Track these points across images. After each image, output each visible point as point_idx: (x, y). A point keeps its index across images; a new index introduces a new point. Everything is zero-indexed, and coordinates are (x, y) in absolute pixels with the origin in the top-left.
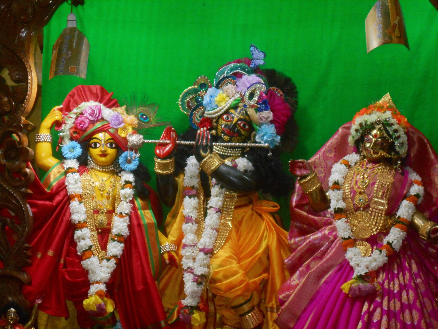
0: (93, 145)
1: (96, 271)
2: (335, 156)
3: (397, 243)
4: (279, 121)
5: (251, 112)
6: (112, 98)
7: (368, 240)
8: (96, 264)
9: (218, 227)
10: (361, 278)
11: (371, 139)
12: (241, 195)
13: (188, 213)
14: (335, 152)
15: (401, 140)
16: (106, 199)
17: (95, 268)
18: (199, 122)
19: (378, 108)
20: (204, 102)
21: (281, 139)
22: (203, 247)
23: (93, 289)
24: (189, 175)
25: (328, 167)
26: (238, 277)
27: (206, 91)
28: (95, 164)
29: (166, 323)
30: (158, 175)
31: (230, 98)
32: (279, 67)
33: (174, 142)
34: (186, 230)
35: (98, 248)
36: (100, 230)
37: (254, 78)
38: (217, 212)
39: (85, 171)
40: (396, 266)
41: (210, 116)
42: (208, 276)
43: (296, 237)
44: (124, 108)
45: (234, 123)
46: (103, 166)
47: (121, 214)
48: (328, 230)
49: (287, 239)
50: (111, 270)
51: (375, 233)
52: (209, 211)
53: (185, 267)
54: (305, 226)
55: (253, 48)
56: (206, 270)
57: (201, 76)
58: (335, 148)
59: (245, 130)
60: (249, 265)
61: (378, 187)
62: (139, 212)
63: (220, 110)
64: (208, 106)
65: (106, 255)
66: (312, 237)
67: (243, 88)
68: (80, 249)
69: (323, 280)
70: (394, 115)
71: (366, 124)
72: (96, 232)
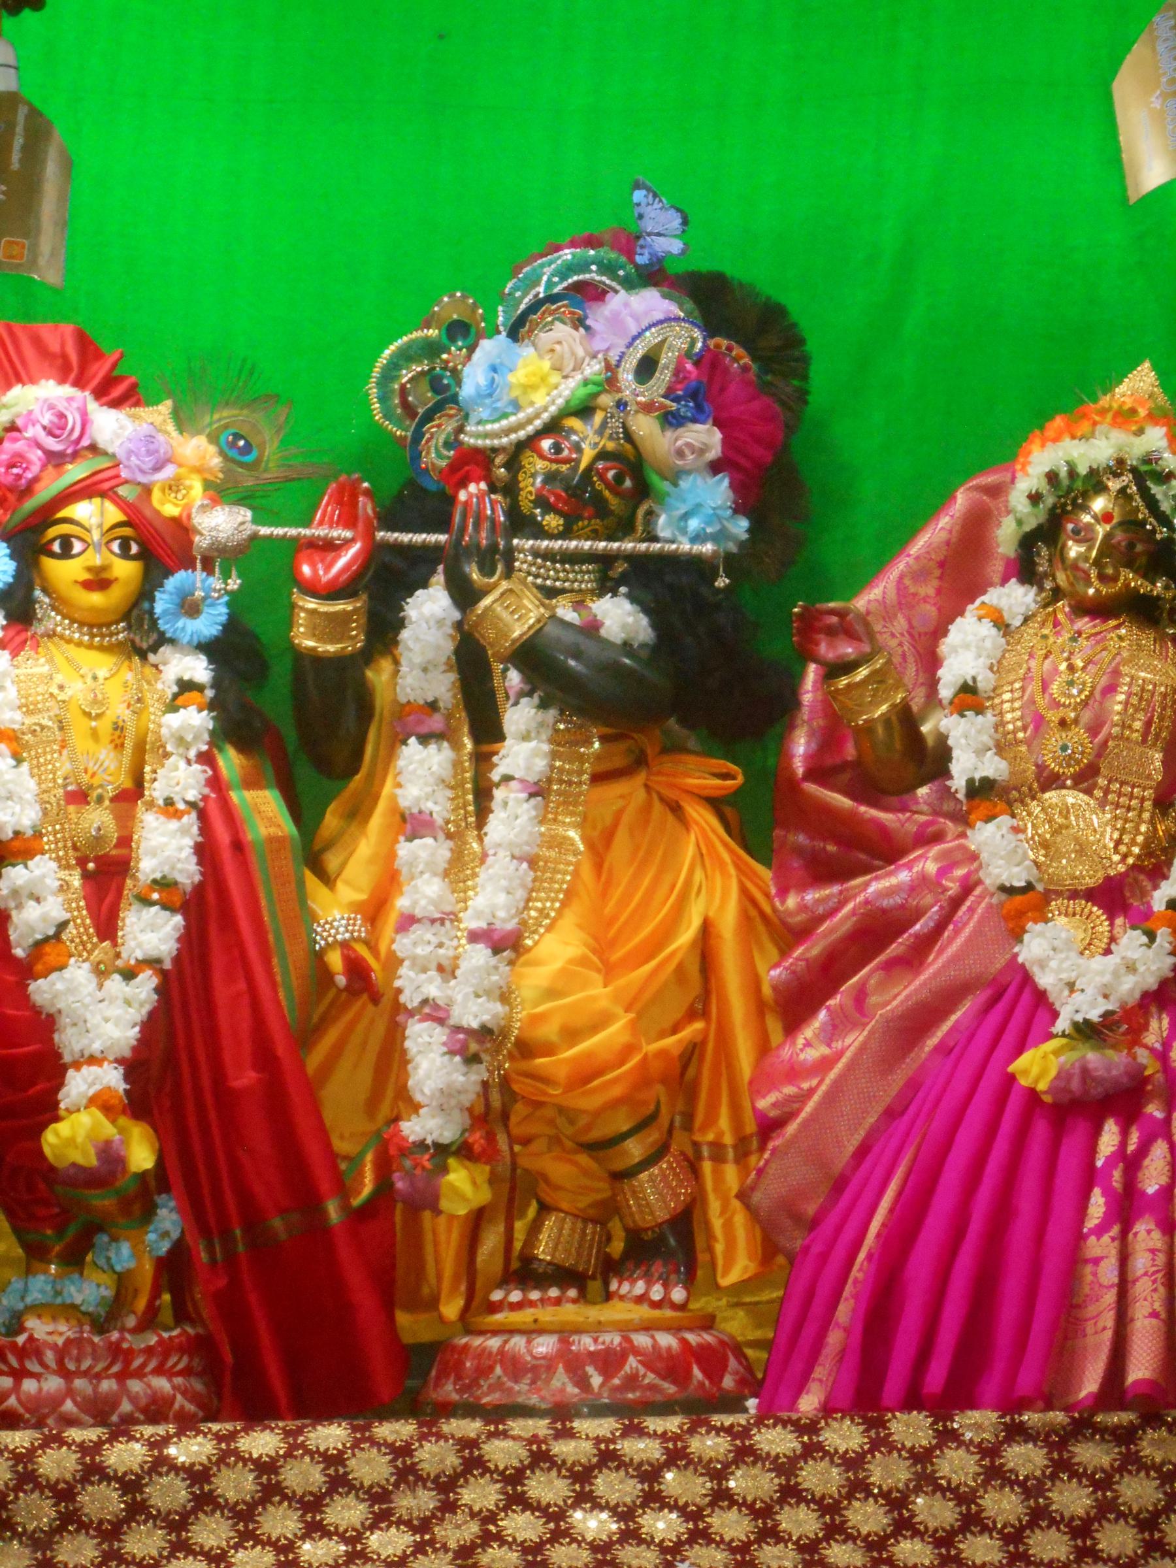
0: (56, 547)
1: (88, 1016)
2: (939, 591)
4: (744, 462)
5: (645, 427)
9: (536, 850)
10: (1086, 1031)
11: (1089, 527)
13: (418, 799)
14: (940, 578)
17: (86, 1006)
18: (443, 463)
20: (467, 391)
21: (749, 531)
23: (78, 1085)
24: (418, 660)
26: (614, 1033)
27: (472, 349)
28: (64, 617)
29: (345, 1206)
30: (302, 658)
31: (565, 377)
32: (755, 271)
33: (369, 535)
34: (411, 865)
35: (86, 930)
36: (91, 866)
37: (651, 303)
38: (532, 795)
39: (25, 642)
42: (505, 1032)
43: (803, 888)
44: (166, 407)
45: (583, 466)
46: (91, 626)
47: (169, 802)
48: (936, 859)
49: (767, 895)
50: (138, 1014)
51: (1121, 868)
52: (499, 794)
53: (410, 999)
54: (831, 848)
55: (644, 192)
56: (499, 1008)
57: (452, 296)
58: (941, 565)
59: (618, 491)
60: (642, 990)
61: (1126, 703)
62: (235, 796)
63: (529, 421)
64: (483, 405)
65: (118, 955)
66: (883, 886)
68: (21, 936)
69: (932, 1042)
72: (77, 873)
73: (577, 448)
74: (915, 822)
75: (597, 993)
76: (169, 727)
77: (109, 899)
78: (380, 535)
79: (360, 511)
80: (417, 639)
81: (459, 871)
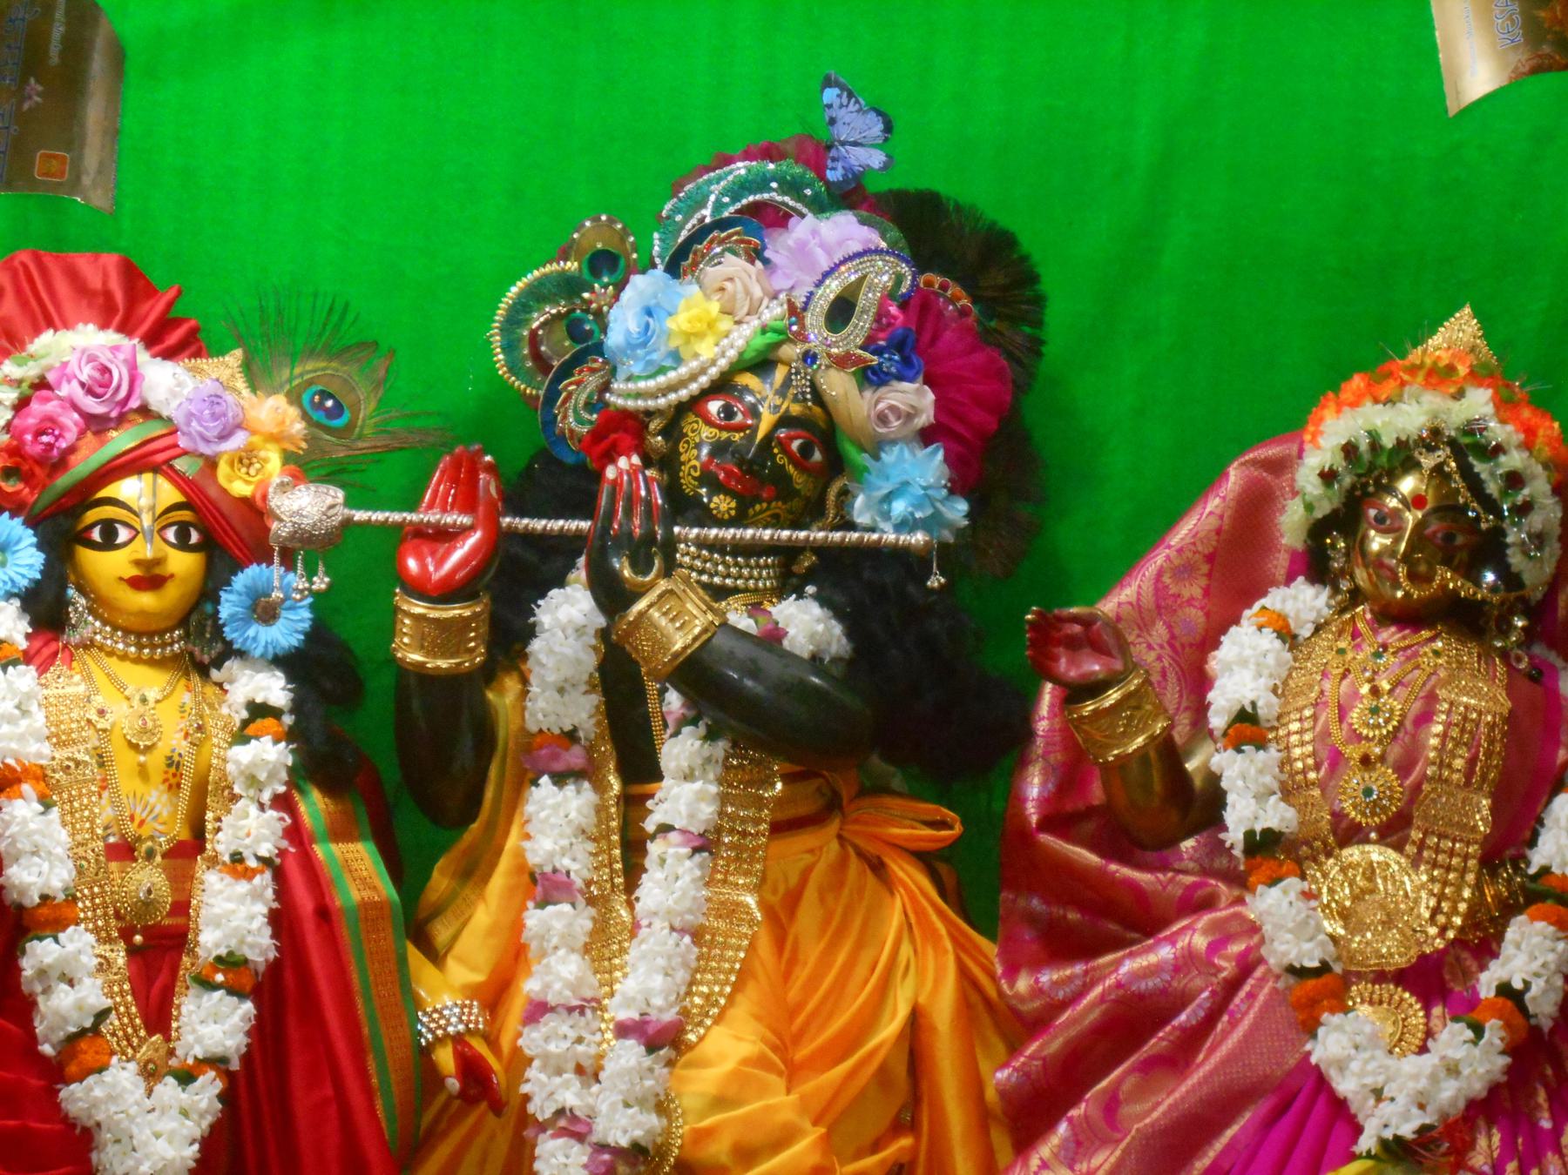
0: (96, 535)
1: (135, 1131)
2: (1207, 592)
3: (1545, 992)
4: (960, 429)
5: (838, 384)
6: (178, 311)
7: (1402, 978)
8: (131, 1100)
12: (797, 768)
13: (551, 855)
15: (1536, 521)
16: (164, 787)
17: (131, 1118)
19: (1431, 372)
20: (614, 339)
21: (969, 515)
22: (634, 1015)
24: (551, 678)
25: (1178, 645)
27: (620, 286)
28: (105, 623)
31: (738, 323)
32: (977, 190)
35: (131, 1020)
36: (138, 938)
37: (844, 231)
38: (696, 850)
39: (55, 654)
40: (1542, 1097)
41: (641, 403)
42: (662, 1151)
43: (1036, 966)
44: (234, 358)
45: (760, 435)
46: (139, 635)
47: (237, 858)
48: (1205, 932)
50: (196, 1128)
52: (654, 848)
53: (541, 1108)
55: (836, 91)
56: (653, 1121)
57: (596, 219)
58: (1210, 558)
59: (805, 465)
61: (1444, 736)
62: (321, 851)
63: (693, 378)
65: (171, 1053)
66: (1139, 964)
67: (798, 275)
68: (52, 1029)
70: (1505, 407)
71: (1375, 446)
73: (753, 412)
74: (1179, 883)
75: (778, 1102)
76: (237, 763)
77: (158, 984)
78: (506, 521)
79: (481, 493)
80: (551, 652)
81: (602, 946)
